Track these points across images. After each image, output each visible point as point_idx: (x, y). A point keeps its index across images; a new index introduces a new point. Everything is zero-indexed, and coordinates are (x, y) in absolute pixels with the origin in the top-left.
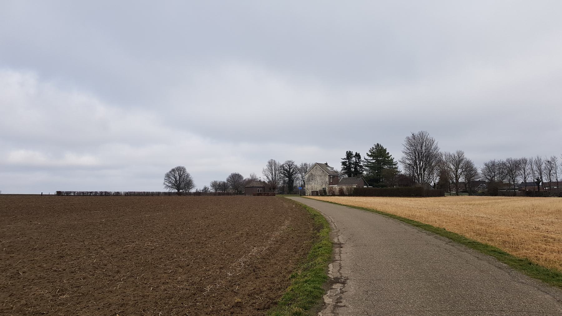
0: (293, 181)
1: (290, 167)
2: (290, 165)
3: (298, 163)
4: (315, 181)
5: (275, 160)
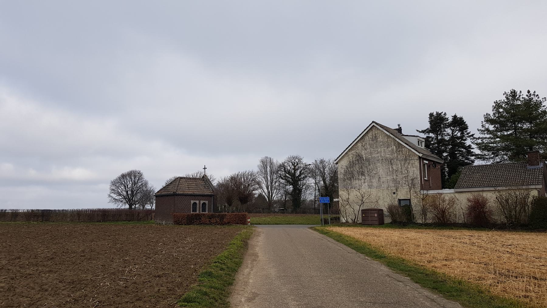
0: (300, 191)
1: (295, 167)
2: (296, 164)
3: (308, 160)
4: (372, 177)
5: (272, 158)
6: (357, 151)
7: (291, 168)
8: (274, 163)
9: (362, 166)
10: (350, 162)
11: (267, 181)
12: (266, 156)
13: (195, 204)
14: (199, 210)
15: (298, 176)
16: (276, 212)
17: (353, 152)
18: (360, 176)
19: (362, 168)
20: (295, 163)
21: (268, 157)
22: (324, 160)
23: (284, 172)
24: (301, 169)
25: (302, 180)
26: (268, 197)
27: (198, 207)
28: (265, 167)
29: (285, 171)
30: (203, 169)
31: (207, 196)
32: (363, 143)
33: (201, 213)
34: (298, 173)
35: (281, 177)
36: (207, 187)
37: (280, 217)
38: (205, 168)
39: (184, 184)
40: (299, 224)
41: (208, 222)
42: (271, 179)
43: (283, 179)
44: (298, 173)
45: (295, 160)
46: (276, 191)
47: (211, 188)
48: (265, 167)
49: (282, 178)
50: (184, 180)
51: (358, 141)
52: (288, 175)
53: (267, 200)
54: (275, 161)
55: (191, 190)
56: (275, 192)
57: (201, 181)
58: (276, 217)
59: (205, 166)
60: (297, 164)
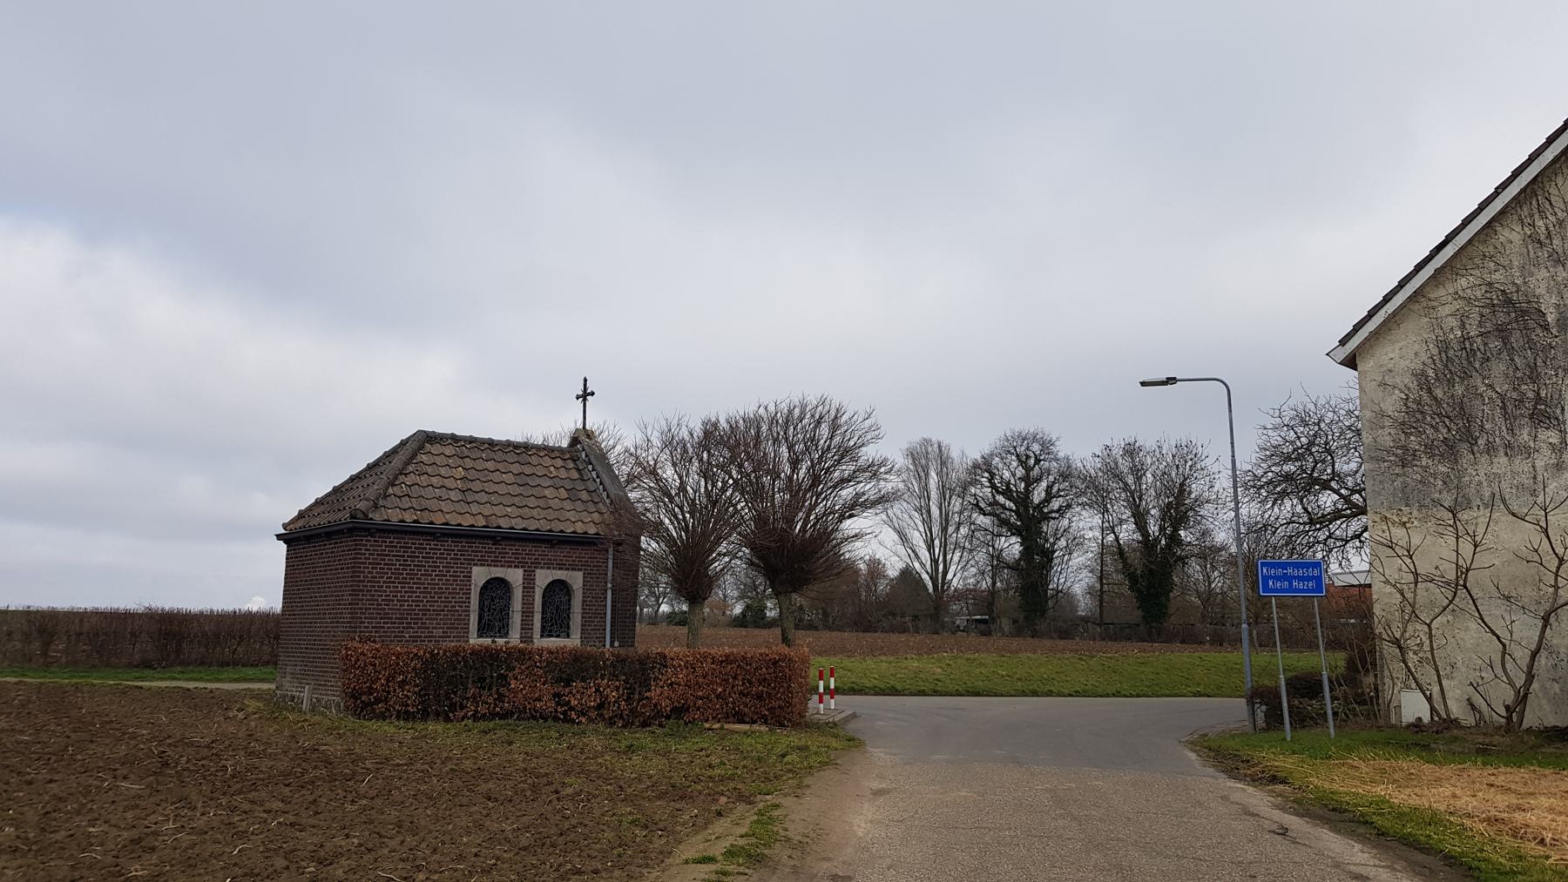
0: (1048, 555)
2: (1032, 461)
6: (1497, 276)
7: (1014, 475)
8: (952, 463)
9: (1533, 368)
10: (1444, 346)
11: (928, 521)
12: (925, 436)
13: (497, 587)
14: (526, 626)
15: (1038, 505)
16: (958, 627)
17: (1463, 282)
18: (1521, 426)
19: (1534, 376)
20: (1028, 457)
21: (931, 441)
22: (1137, 445)
23: (990, 490)
24: (1051, 478)
25: (1054, 518)
26: (931, 578)
27: (517, 604)
28: (922, 474)
29: (993, 486)
30: (593, 394)
31: (577, 543)
32: (1540, 223)
33: (475, 640)
34: (1038, 495)
35: (977, 505)
36: (584, 496)
37: (984, 657)
38: (585, 395)
39: (443, 471)
40: (1077, 694)
41: (547, 704)
42: (941, 512)
43: (985, 515)
44: (1038, 495)
45: (1028, 448)
46: (961, 557)
47: (608, 501)
48: (922, 474)
49: (981, 509)
50: (449, 451)
51: (1503, 212)
52: (1001, 499)
53: (927, 590)
54: (955, 454)
55: (475, 509)
56: (956, 558)
57: (559, 463)
58: (968, 659)
59: (585, 380)
60: (1038, 461)
